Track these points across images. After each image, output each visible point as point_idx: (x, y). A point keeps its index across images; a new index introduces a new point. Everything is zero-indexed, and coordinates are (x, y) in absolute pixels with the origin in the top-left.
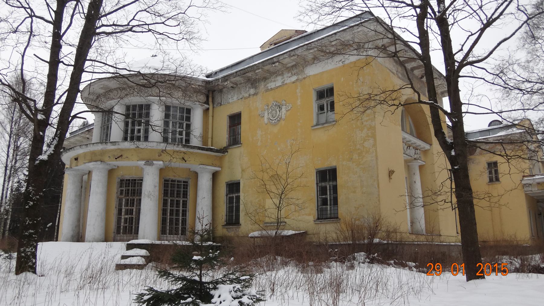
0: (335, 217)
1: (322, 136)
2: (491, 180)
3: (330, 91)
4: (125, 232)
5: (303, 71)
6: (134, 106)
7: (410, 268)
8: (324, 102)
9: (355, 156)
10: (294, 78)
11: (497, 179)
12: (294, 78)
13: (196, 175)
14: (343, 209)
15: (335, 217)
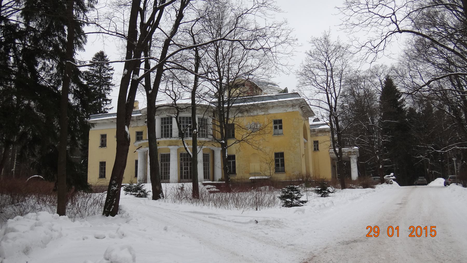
0: (283, 171)
1: (277, 139)
2: (315, 150)
3: (280, 121)
4: (185, 178)
5: (267, 111)
6: (165, 118)
7: (34, 209)
8: (278, 125)
9: (292, 149)
10: (263, 113)
11: (318, 150)
12: (263, 113)
13: (213, 152)
14: (287, 168)
15: (283, 171)
